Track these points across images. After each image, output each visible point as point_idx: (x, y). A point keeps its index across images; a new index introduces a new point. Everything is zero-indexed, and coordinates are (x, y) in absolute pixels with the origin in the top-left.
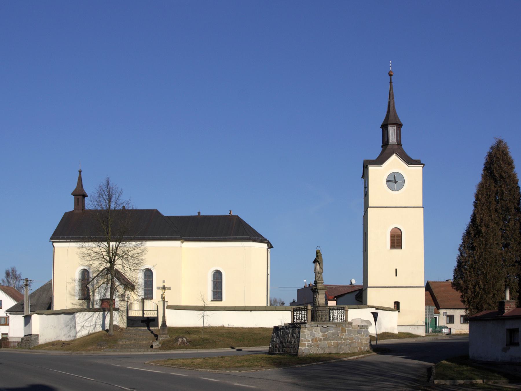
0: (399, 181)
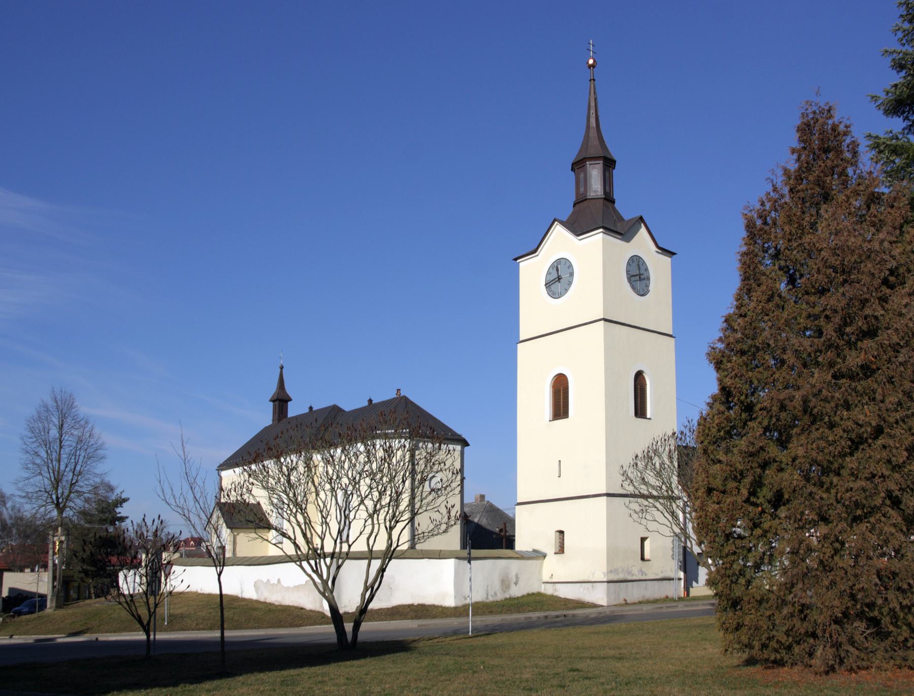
0: (565, 276)
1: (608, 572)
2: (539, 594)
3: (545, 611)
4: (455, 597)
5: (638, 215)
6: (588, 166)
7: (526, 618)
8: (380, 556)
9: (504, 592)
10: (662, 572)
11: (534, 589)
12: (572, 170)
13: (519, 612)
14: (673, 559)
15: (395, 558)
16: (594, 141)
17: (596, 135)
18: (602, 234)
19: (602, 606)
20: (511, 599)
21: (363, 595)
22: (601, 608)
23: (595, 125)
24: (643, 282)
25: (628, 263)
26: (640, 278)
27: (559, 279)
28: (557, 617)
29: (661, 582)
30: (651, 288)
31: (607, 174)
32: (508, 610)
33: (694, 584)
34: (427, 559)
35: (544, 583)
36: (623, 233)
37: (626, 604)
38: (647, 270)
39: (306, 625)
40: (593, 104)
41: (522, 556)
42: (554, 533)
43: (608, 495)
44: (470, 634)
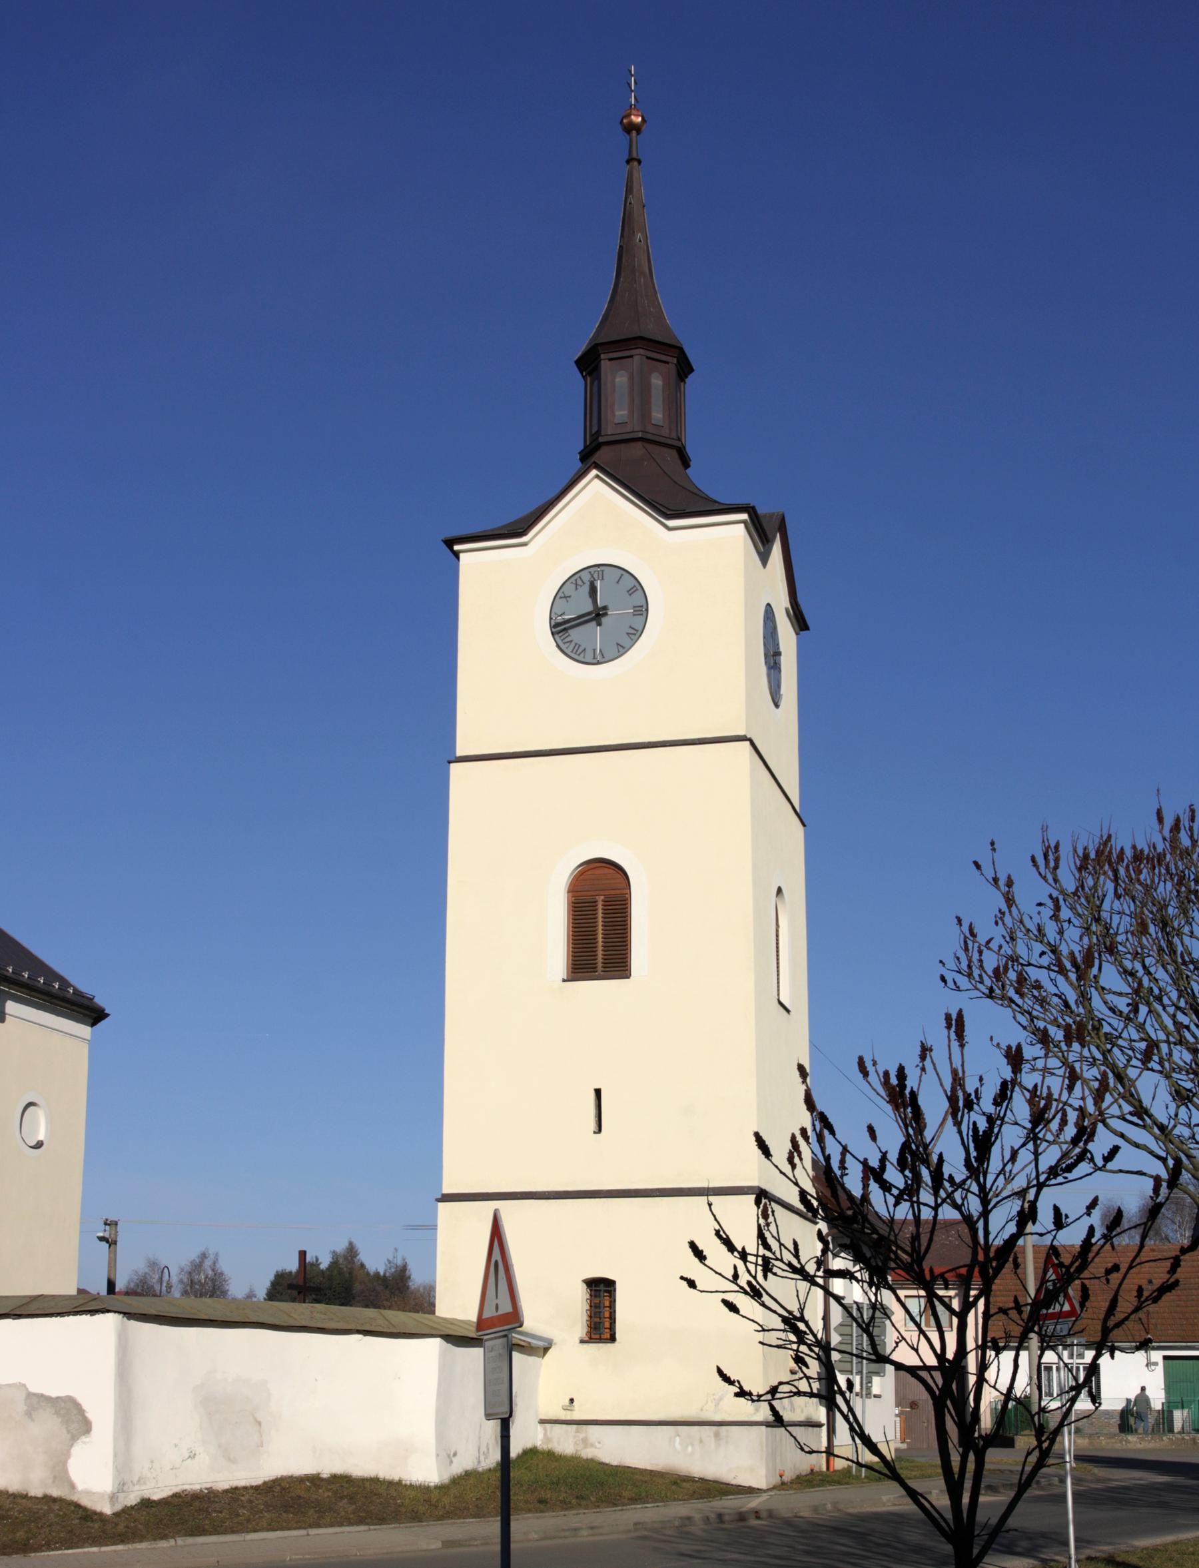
0: (618, 612)
35: (542, 1422)
39: (49, 1546)
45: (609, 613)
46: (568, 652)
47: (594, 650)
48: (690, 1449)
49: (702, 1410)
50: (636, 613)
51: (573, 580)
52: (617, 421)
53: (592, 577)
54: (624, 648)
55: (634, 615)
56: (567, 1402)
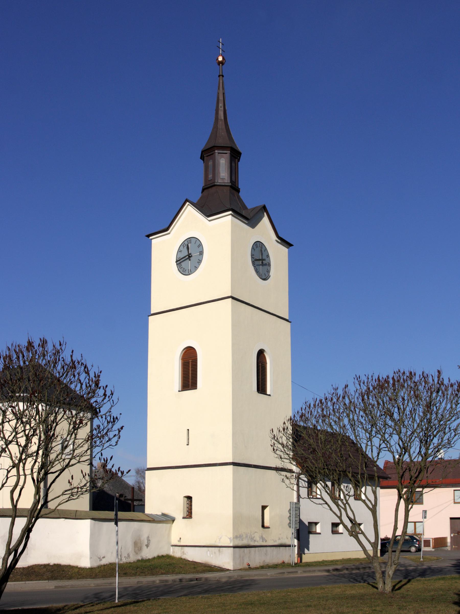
0: (195, 254)
1: (234, 538)
2: (168, 557)
3: (177, 573)
4: (91, 558)
5: (261, 204)
6: (217, 154)
7: (161, 581)
8: (27, 515)
9: (137, 553)
10: (279, 539)
11: (163, 552)
12: (201, 158)
13: (153, 574)
14: (290, 527)
15: (42, 517)
16: (222, 132)
17: (224, 127)
18: (230, 216)
19: (228, 570)
20: (143, 561)
21: (5, 560)
22: (228, 572)
23: (223, 118)
24: (265, 267)
25: (253, 248)
26: (262, 263)
27: (189, 256)
28: (191, 580)
29: (278, 548)
30: (272, 273)
31: (233, 164)
32: (142, 572)
33: (306, 550)
34: (64, 519)
35: (173, 546)
36: (249, 218)
37: (250, 568)
38: (268, 256)
40: (221, 98)
41: (152, 520)
42: (182, 498)
43: (234, 464)
44: (117, 601)
45: (193, 255)
46: (181, 271)
47: (188, 270)
48: (212, 555)
49: (215, 542)
50: (200, 254)
51: (182, 245)
52: (209, 180)
53: (188, 242)
54: (197, 268)
55: (200, 255)
56: (179, 539)
